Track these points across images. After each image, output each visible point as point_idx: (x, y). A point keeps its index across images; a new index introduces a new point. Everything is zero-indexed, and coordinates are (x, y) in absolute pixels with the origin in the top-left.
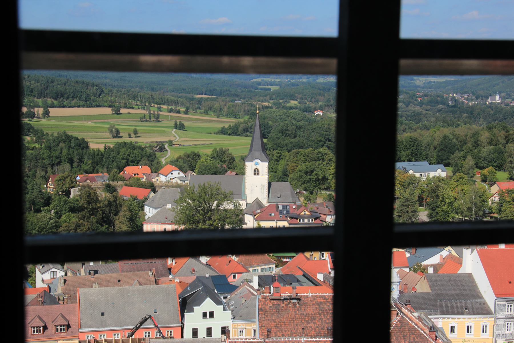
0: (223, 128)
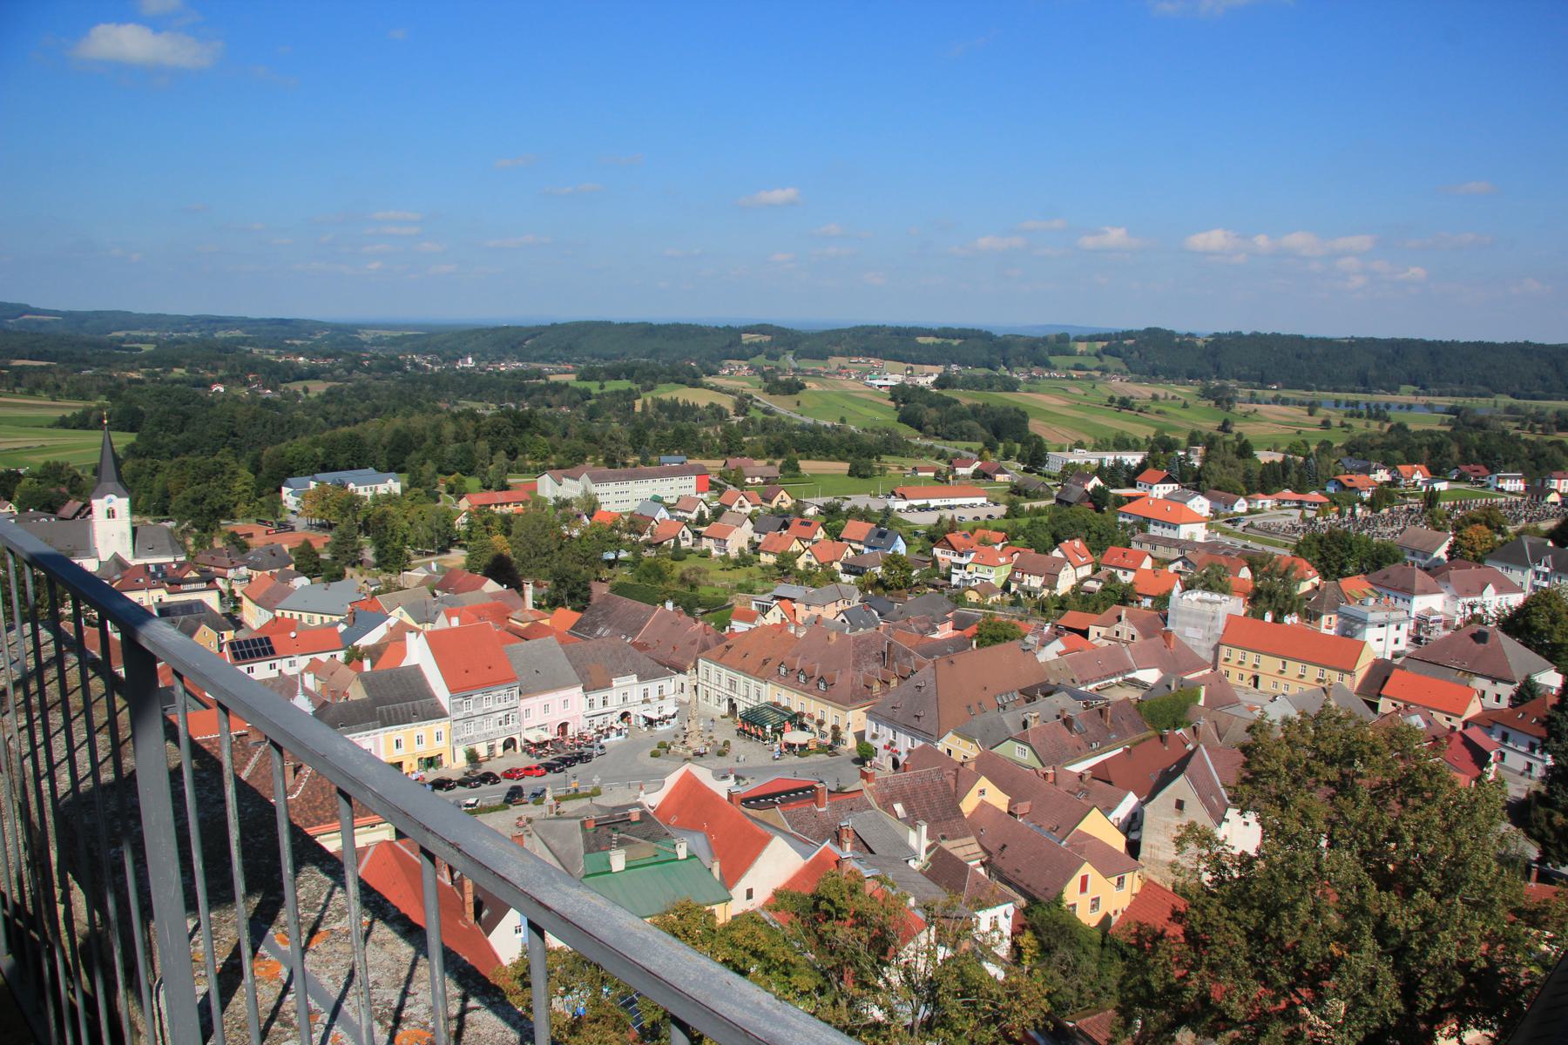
0: (63, 418)
